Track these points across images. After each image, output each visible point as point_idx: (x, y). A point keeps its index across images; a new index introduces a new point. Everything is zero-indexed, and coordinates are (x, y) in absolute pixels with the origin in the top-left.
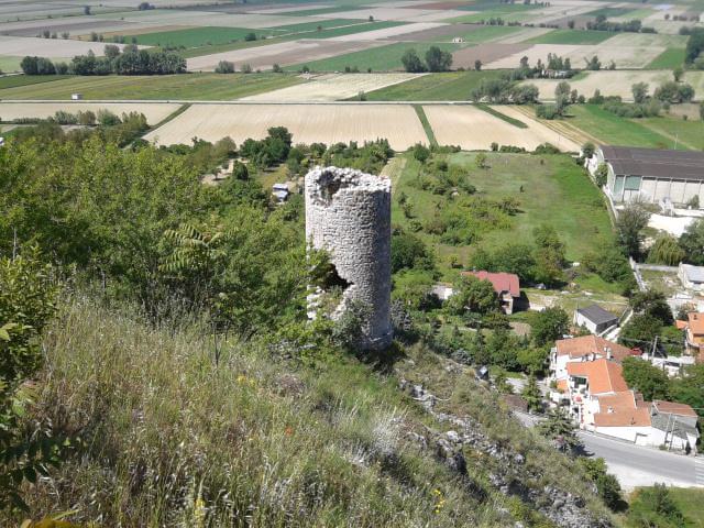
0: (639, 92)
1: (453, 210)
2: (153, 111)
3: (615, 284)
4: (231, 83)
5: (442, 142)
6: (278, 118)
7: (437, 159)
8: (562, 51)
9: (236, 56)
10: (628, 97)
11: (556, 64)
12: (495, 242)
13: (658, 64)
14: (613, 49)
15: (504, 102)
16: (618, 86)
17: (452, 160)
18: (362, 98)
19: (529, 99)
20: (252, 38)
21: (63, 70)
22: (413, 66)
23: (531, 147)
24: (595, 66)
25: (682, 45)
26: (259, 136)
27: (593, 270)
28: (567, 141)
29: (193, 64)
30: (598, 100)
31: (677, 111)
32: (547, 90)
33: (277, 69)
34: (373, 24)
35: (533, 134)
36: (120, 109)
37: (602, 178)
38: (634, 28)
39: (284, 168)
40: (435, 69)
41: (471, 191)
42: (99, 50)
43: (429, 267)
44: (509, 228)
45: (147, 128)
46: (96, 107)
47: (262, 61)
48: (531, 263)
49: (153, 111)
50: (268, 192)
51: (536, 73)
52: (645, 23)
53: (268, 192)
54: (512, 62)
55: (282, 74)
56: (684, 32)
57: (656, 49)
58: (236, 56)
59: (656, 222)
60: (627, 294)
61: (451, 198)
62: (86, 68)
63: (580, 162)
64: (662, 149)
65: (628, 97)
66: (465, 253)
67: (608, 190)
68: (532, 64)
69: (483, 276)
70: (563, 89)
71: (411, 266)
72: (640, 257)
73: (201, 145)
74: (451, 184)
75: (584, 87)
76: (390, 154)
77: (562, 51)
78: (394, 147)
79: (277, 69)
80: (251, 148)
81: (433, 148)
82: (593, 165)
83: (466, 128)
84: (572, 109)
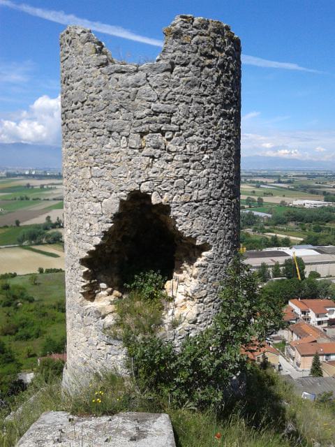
1: (20, 315)
15: (40, 243)
17: (12, 282)
41: (31, 301)
54: (41, 220)
61: (17, 308)
68: (54, 220)
74: (15, 298)
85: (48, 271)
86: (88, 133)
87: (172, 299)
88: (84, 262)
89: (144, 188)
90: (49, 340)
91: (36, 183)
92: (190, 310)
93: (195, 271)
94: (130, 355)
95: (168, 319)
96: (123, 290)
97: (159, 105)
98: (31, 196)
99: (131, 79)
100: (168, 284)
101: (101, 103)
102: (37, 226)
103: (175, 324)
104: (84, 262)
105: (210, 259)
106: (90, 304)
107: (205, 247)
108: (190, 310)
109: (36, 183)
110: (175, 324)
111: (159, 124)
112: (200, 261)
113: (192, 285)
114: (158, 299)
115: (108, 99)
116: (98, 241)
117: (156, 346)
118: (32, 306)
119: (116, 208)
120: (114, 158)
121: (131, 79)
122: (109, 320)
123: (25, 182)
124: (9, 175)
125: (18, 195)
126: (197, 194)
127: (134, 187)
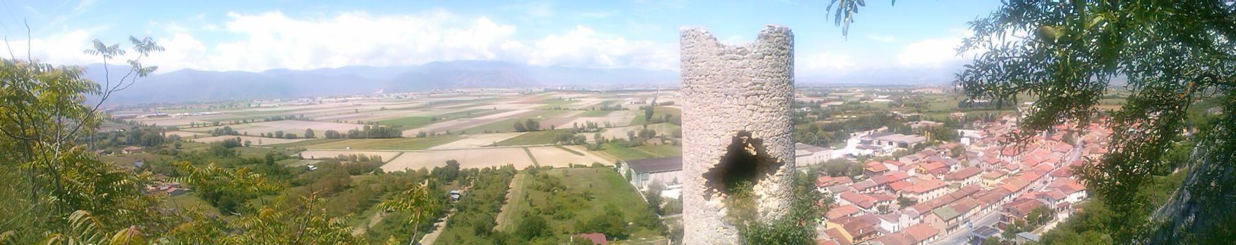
0: (631, 135)
1: (557, 199)
2: (385, 155)
3: (655, 231)
4: (425, 141)
5: (542, 165)
6: (452, 156)
7: (541, 173)
8: (593, 120)
9: (427, 129)
10: (627, 138)
11: (591, 126)
12: (585, 216)
13: (633, 123)
14: (614, 118)
15: (570, 144)
16: (622, 134)
17: (550, 173)
18: (495, 145)
19: (581, 142)
20: (434, 120)
21: (343, 137)
22: (519, 128)
23: (590, 164)
24: (608, 126)
25: (643, 113)
26: (442, 165)
27: (642, 225)
28: (606, 161)
29: (405, 133)
30: (615, 141)
31: (651, 142)
32: (590, 138)
33: (448, 133)
34: (496, 111)
35: (588, 159)
36: (369, 154)
37: (629, 177)
38: (618, 108)
39: (456, 182)
40: (531, 130)
41: (564, 189)
42: (361, 128)
43: (550, 234)
44: (587, 207)
45: (383, 164)
46: (357, 153)
47: (442, 129)
48: (609, 226)
49: (385, 155)
50: (448, 196)
51: (582, 130)
52: (623, 106)
53: (448, 196)
54: (570, 125)
55: (450, 135)
56: (641, 108)
57: (632, 117)
58: (427, 129)
59: (665, 194)
60: (663, 234)
61: (554, 194)
62: (354, 135)
63: (616, 170)
64: (651, 158)
65: (627, 138)
66: (569, 224)
67: (633, 183)
68: (579, 126)
69: (585, 236)
70: (597, 137)
71: (539, 235)
72: (662, 213)
73: (410, 172)
74: (553, 185)
75: (609, 135)
76: (515, 172)
77: (593, 120)
78: (518, 168)
79: (448, 133)
80: (438, 172)
81: (538, 167)
82: (623, 171)
83: (553, 158)
84: (604, 146)
85: (577, 166)
86: (710, 95)
87: (760, 197)
88: (705, 175)
89: (748, 129)
90: (579, 222)
91: (566, 96)
92: (774, 204)
93: (777, 179)
94: (740, 234)
95: (760, 210)
96: (727, 192)
97: (756, 79)
98: (562, 107)
99: (740, 63)
100: (755, 188)
101: (721, 77)
102: (567, 130)
103: (765, 213)
104: (705, 175)
105: (784, 171)
106: (708, 203)
107: (782, 163)
108: (774, 204)
109: (566, 96)
110: (765, 213)
111: (756, 91)
112: (778, 172)
113: (775, 187)
114: (749, 197)
115: (725, 75)
116: (717, 162)
117: (754, 225)
118: (565, 193)
119: (730, 142)
120: (729, 111)
121: (740, 63)
122: (723, 212)
123: (558, 95)
124: (546, 91)
125: (553, 105)
126: (778, 131)
127: (742, 128)
